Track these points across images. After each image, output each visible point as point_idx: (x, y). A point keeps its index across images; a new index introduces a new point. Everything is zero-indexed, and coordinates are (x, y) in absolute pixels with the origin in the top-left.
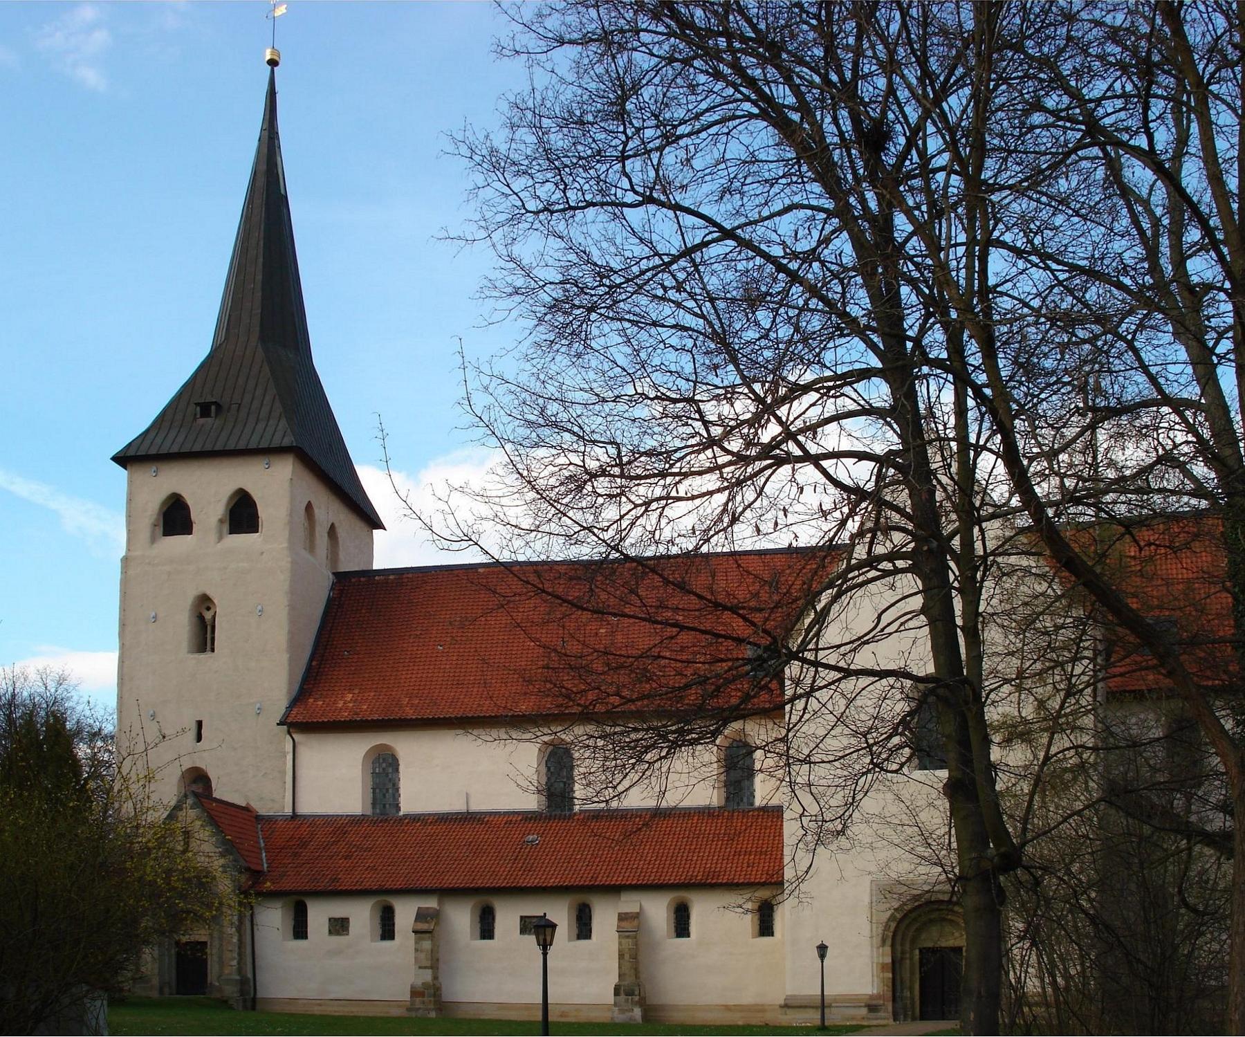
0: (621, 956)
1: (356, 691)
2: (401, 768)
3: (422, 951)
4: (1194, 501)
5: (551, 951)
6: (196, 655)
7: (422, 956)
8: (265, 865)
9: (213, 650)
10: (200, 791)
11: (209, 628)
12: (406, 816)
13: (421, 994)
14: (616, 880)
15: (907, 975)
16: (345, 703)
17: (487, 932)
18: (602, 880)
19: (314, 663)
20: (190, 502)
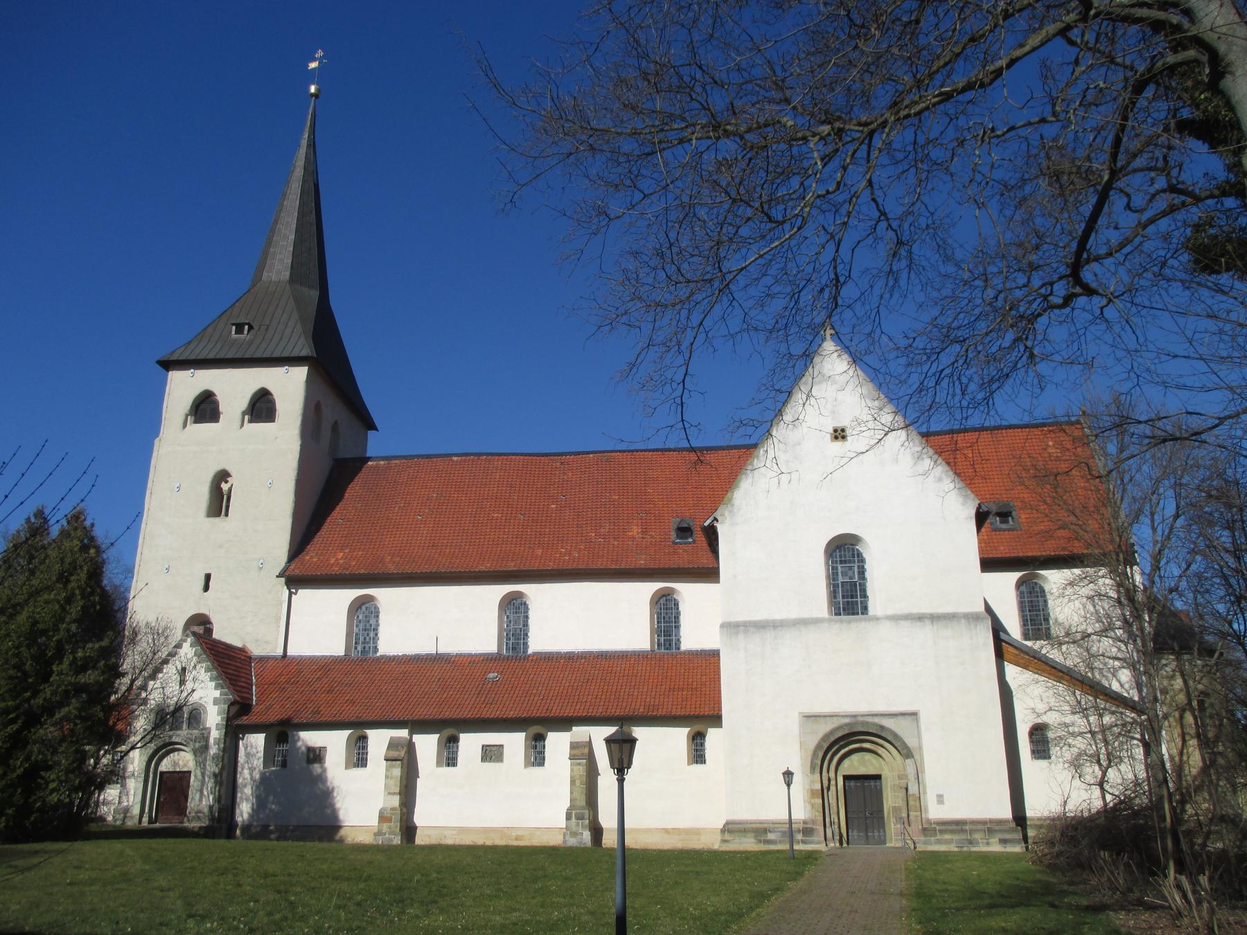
0: (573, 782)
1: (347, 551)
2: (381, 616)
3: (391, 778)
5: (630, 776)
6: (212, 519)
7: (392, 782)
9: (227, 515)
10: (201, 632)
11: (225, 497)
13: (389, 820)
14: (569, 712)
15: (833, 801)
16: (338, 560)
17: (451, 761)
18: (556, 711)
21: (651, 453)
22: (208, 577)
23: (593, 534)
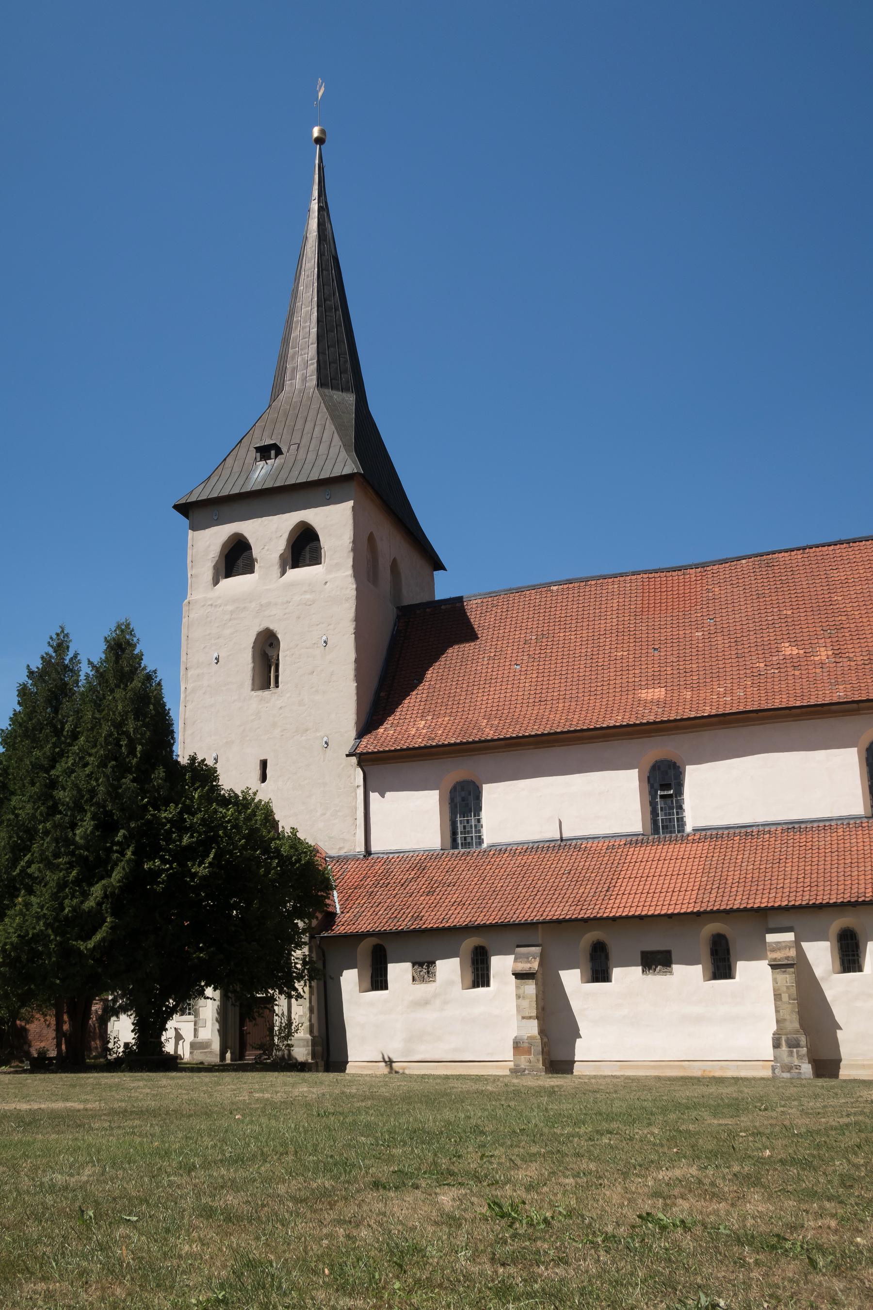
0: (777, 997)
1: (429, 718)
4: (278, 1024)
7: (525, 1003)
8: (338, 906)
12: (491, 846)
19: (382, 694)
20: (252, 541)
21: (832, 547)
22: (264, 764)
23: (762, 665)
